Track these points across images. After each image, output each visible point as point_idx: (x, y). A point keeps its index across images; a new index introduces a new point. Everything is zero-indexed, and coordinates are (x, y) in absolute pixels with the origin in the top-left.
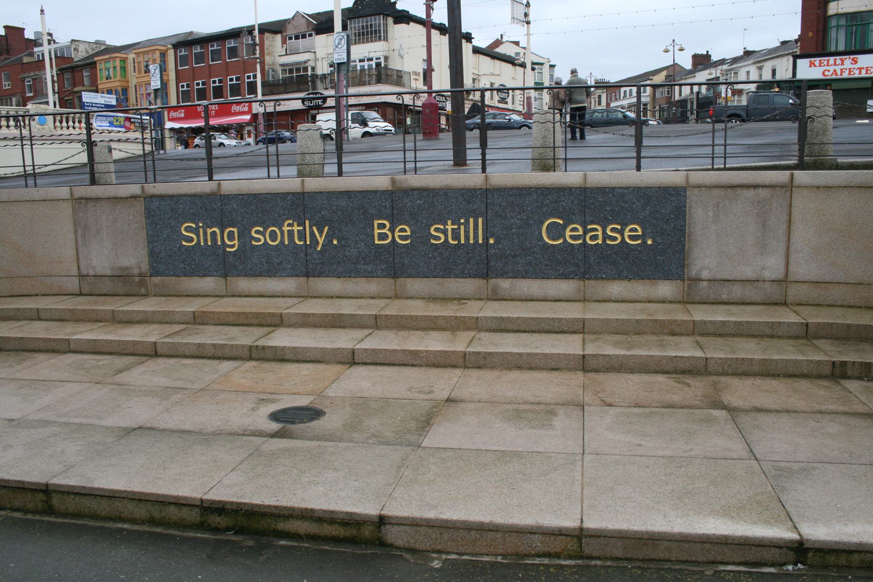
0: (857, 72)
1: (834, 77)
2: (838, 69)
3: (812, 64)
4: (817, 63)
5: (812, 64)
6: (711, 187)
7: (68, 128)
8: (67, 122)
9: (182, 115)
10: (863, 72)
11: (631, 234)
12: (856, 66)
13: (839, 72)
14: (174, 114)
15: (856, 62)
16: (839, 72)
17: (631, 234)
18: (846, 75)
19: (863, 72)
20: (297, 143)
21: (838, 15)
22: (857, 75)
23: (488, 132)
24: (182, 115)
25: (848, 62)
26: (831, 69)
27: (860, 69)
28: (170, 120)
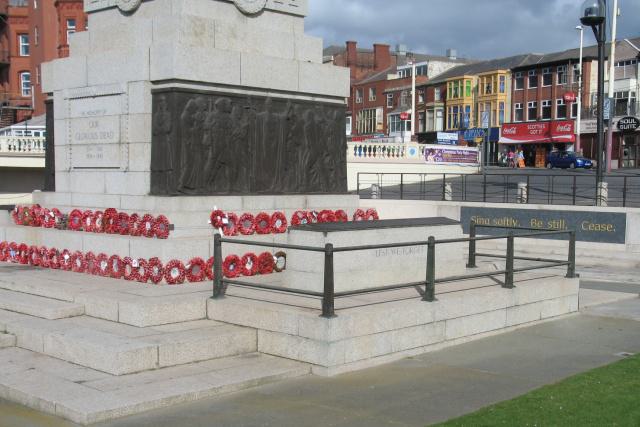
9: (514, 132)
11: (608, 228)
14: (507, 131)
17: (608, 228)
24: (514, 132)
28: (503, 135)
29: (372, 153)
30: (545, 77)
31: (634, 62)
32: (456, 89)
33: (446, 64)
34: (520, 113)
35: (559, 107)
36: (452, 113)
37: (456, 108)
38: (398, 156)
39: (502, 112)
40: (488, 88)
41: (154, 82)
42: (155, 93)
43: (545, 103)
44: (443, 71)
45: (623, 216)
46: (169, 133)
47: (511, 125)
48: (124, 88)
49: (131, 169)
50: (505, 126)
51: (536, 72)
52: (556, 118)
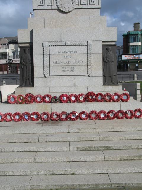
2: (130, 57)
3: (125, 56)
5: (125, 56)
18: (132, 59)
21: (132, 46)
25: (132, 56)
26: (129, 57)
31: (7, 44)
41: (103, 42)
42: (103, 46)
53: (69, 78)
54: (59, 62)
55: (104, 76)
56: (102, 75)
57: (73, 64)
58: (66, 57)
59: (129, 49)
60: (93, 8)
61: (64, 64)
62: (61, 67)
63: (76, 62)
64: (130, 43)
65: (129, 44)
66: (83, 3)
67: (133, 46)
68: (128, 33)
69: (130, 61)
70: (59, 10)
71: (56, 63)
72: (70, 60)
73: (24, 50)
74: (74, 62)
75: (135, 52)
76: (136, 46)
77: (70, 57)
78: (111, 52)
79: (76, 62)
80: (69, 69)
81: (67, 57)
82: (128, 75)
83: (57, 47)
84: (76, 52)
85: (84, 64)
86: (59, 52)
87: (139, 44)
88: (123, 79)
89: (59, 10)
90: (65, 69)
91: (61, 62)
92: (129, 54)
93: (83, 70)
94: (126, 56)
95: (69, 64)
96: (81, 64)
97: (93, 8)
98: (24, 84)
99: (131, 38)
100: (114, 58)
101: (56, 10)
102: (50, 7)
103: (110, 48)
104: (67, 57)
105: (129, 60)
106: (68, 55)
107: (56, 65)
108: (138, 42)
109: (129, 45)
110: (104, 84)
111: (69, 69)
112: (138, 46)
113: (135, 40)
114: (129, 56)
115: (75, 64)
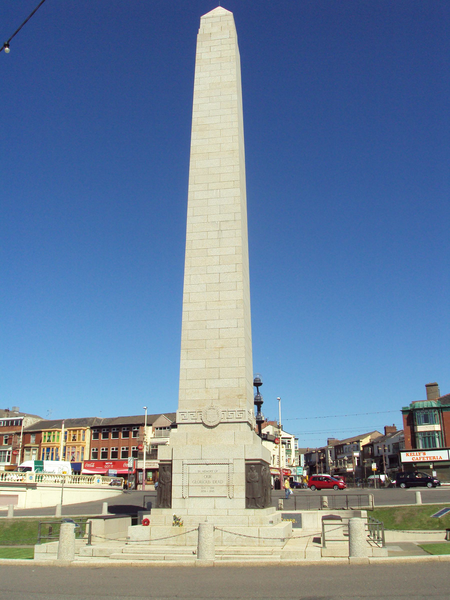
0: (426, 459)
1: (417, 461)
2: (418, 457)
3: (407, 455)
4: (409, 454)
5: (407, 455)
6: (443, 421)
7: (38, 481)
8: (76, 480)
9: (93, 466)
10: (429, 458)
12: (425, 456)
13: (419, 459)
14: (88, 465)
15: (425, 454)
16: (419, 459)
18: (422, 460)
19: (429, 458)
20: (184, 527)
21: (421, 432)
22: (426, 460)
23: (151, 473)
24: (93, 466)
25: (422, 453)
26: (416, 457)
27: (427, 457)
28: (85, 468)
29: (40, 479)
30: (103, 434)
31: (168, 428)
32: (49, 437)
33: (35, 419)
34: (95, 455)
35: (102, 452)
36: (45, 452)
37: (48, 449)
38: (41, 481)
39: (83, 453)
40: (74, 437)
41: (246, 460)
42: (247, 464)
43: (123, 449)
44: (33, 423)
45: (300, 515)
46: (257, 482)
47: (89, 462)
48: (231, 461)
49: (235, 497)
50: (86, 462)
51: (117, 430)
52: (101, 459)
53: (209, 499)
54: (198, 482)
55: (247, 498)
56: (244, 496)
57: (213, 484)
58: (205, 477)
59: (417, 439)
60: (240, 422)
61: (203, 484)
62: (200, 487)
63: (216, 482)
64: (416, 425)
65: (415, 427)
66: (229, 417)
67: (424, 432)
68: (411, 405)
69: (418, 465)
70: (203, 423)
71: (195, 483)
72: (210, 479)
73: (163, 468)
74: (214, 482)
75: (430, 447)
76: (429, 432)
77: (210, 477)
78: (255, 471)
79: (216, 482)
80: (209, 490)
81: (207, 477)
82: (356, 497)
83: (197, 465)
84: (217, 471)
85: (225, 485)
86: (199, 471)
87: (437, 427)
88: (349, 504)
89: (203, 423)
90: (204, 490)
91: (200, 482)
92: (418, 448)
93: (222, 491)
94: (409, 453)
95: (209, 484)
96: (222, 484)
97: (240, 422)
98: (162, 504)
99: (419, 415)
100: (258, 477)
101: (202, 425)
102: (194, 421)
103: (253, 466)
104: (207, 477)
105: (415, 463)
106: (208, 475)
107: (195, 484)
108: (433, 423)
109: (415, 431)
110: (247, 507)
111: (209, 490)
112: (433, 432)
113: (427, 421)
114: (415, 454)
115: (215, 484)
